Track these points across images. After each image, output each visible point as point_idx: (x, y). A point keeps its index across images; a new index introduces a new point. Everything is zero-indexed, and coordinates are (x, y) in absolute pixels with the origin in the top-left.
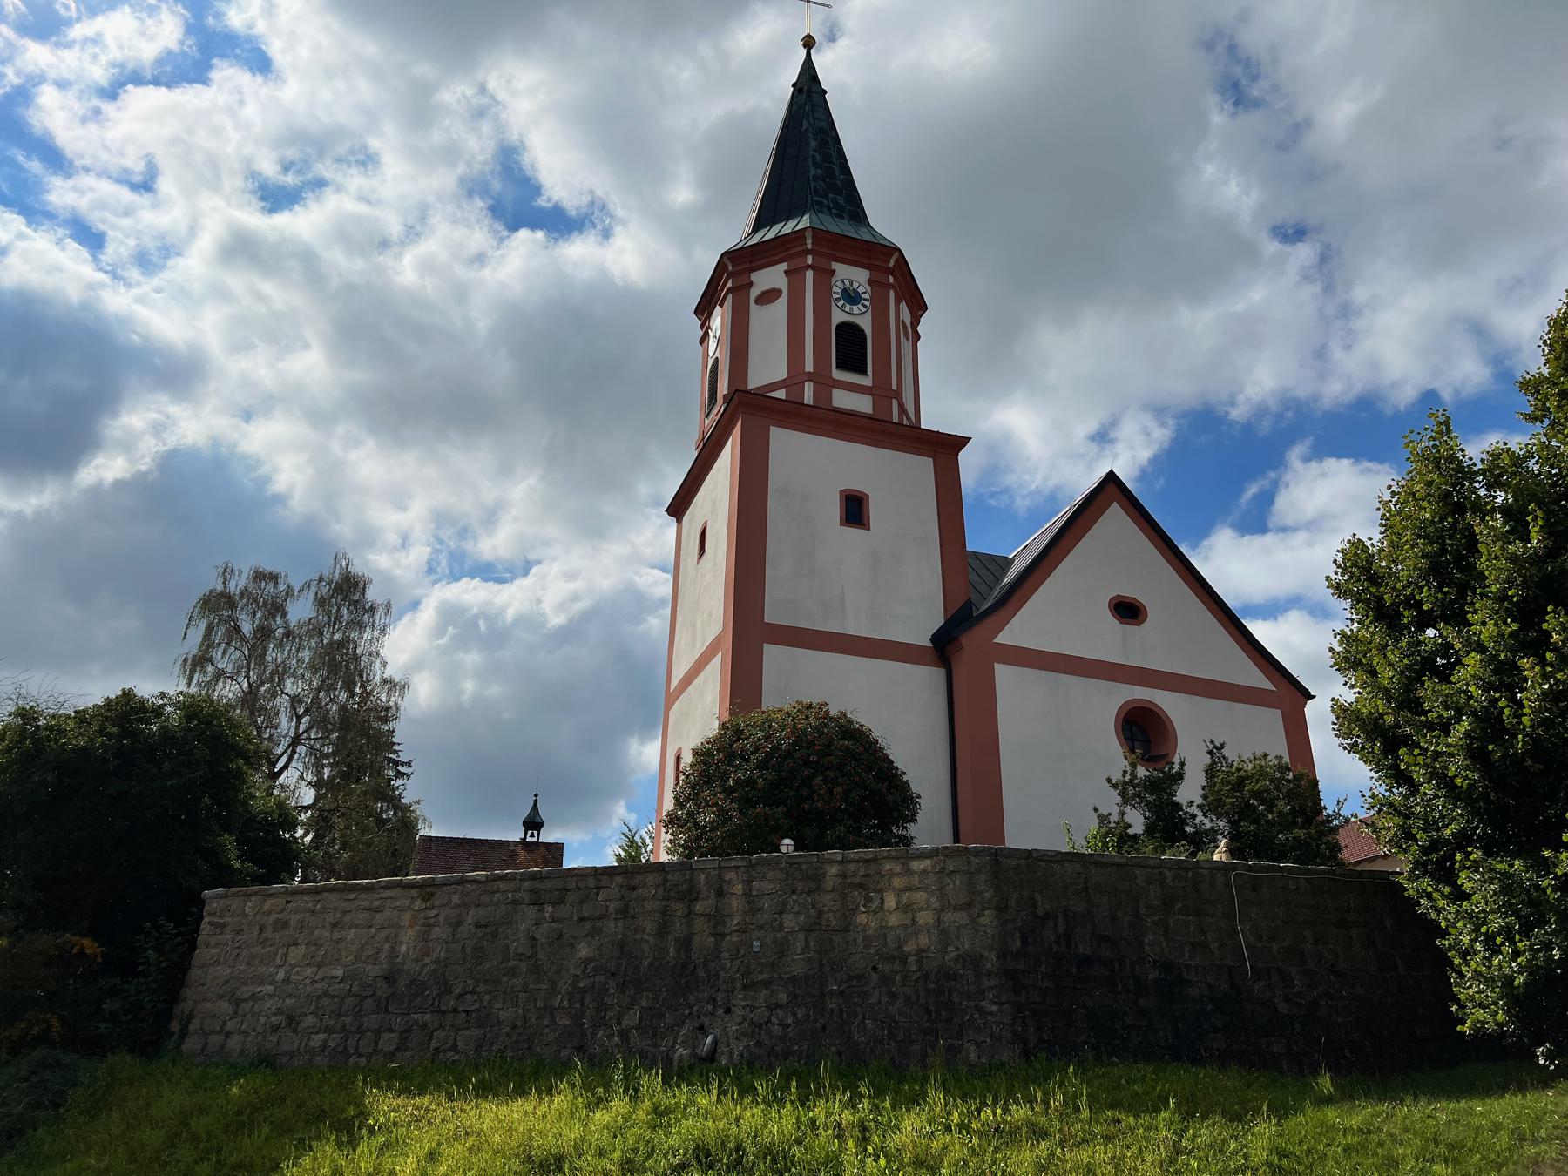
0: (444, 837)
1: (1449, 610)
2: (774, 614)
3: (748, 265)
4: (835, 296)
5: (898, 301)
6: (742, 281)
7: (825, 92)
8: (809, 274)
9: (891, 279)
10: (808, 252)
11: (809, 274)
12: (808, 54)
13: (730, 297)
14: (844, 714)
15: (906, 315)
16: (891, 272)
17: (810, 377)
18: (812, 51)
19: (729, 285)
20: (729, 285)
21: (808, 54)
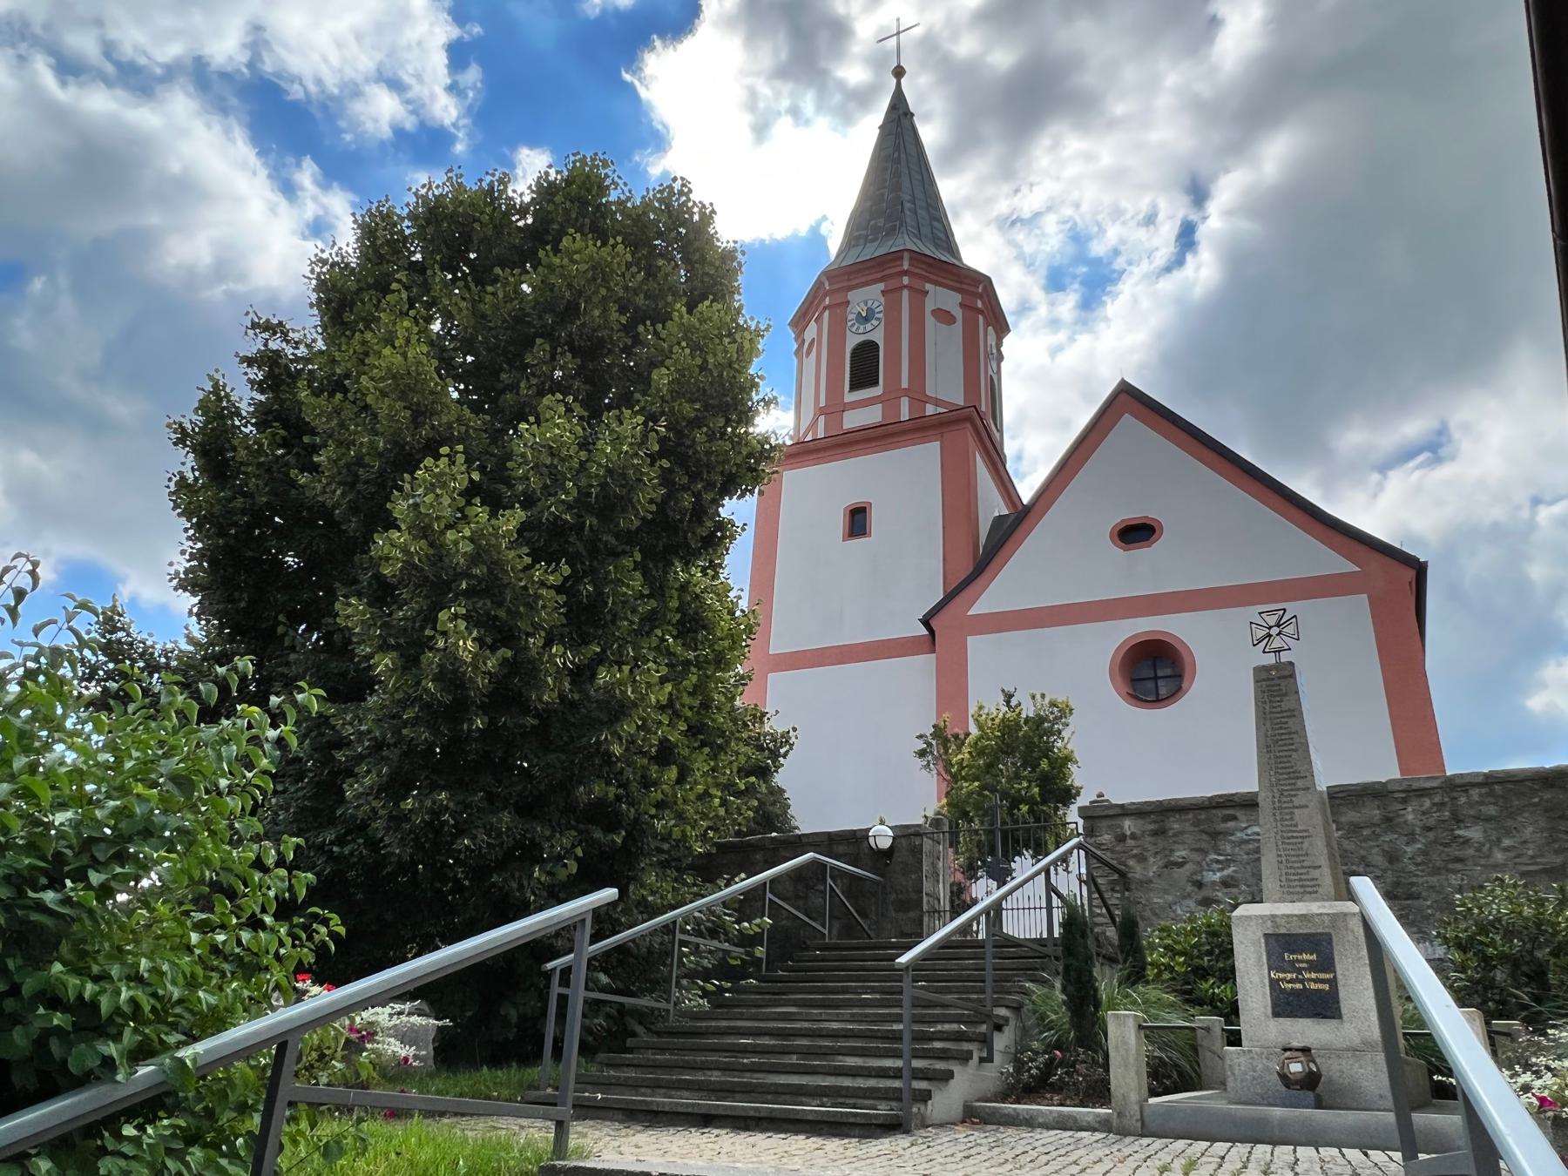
0: (1400, 918)
1: (286, 538)
2: (924, 664)
3: (845, 284)
4: (881, 308)
5: (987, 324)
6: (839, 299)
7: (912, 115)
8: (905, 293)
9: (980, 304)
10: (905, 273)
11: (905, 293)
12: (899, 85)
13: (826, 314)
14: (1068, 759)
15: (992, 340)
16: (980, 296)
17: (906, 392)
18: (903, 81)
19: (827, 301)
20: (827, 301)
21: (899, 85)
